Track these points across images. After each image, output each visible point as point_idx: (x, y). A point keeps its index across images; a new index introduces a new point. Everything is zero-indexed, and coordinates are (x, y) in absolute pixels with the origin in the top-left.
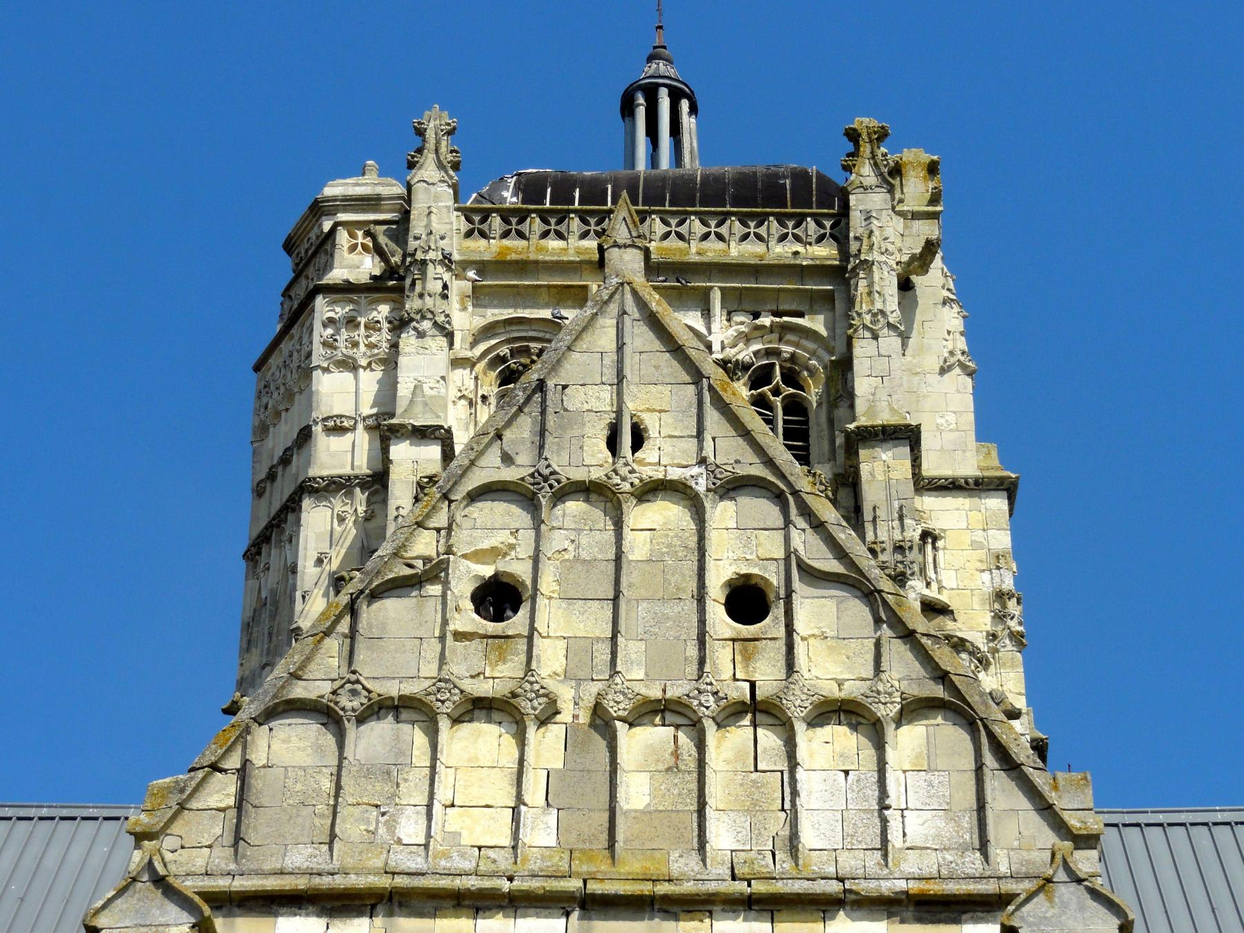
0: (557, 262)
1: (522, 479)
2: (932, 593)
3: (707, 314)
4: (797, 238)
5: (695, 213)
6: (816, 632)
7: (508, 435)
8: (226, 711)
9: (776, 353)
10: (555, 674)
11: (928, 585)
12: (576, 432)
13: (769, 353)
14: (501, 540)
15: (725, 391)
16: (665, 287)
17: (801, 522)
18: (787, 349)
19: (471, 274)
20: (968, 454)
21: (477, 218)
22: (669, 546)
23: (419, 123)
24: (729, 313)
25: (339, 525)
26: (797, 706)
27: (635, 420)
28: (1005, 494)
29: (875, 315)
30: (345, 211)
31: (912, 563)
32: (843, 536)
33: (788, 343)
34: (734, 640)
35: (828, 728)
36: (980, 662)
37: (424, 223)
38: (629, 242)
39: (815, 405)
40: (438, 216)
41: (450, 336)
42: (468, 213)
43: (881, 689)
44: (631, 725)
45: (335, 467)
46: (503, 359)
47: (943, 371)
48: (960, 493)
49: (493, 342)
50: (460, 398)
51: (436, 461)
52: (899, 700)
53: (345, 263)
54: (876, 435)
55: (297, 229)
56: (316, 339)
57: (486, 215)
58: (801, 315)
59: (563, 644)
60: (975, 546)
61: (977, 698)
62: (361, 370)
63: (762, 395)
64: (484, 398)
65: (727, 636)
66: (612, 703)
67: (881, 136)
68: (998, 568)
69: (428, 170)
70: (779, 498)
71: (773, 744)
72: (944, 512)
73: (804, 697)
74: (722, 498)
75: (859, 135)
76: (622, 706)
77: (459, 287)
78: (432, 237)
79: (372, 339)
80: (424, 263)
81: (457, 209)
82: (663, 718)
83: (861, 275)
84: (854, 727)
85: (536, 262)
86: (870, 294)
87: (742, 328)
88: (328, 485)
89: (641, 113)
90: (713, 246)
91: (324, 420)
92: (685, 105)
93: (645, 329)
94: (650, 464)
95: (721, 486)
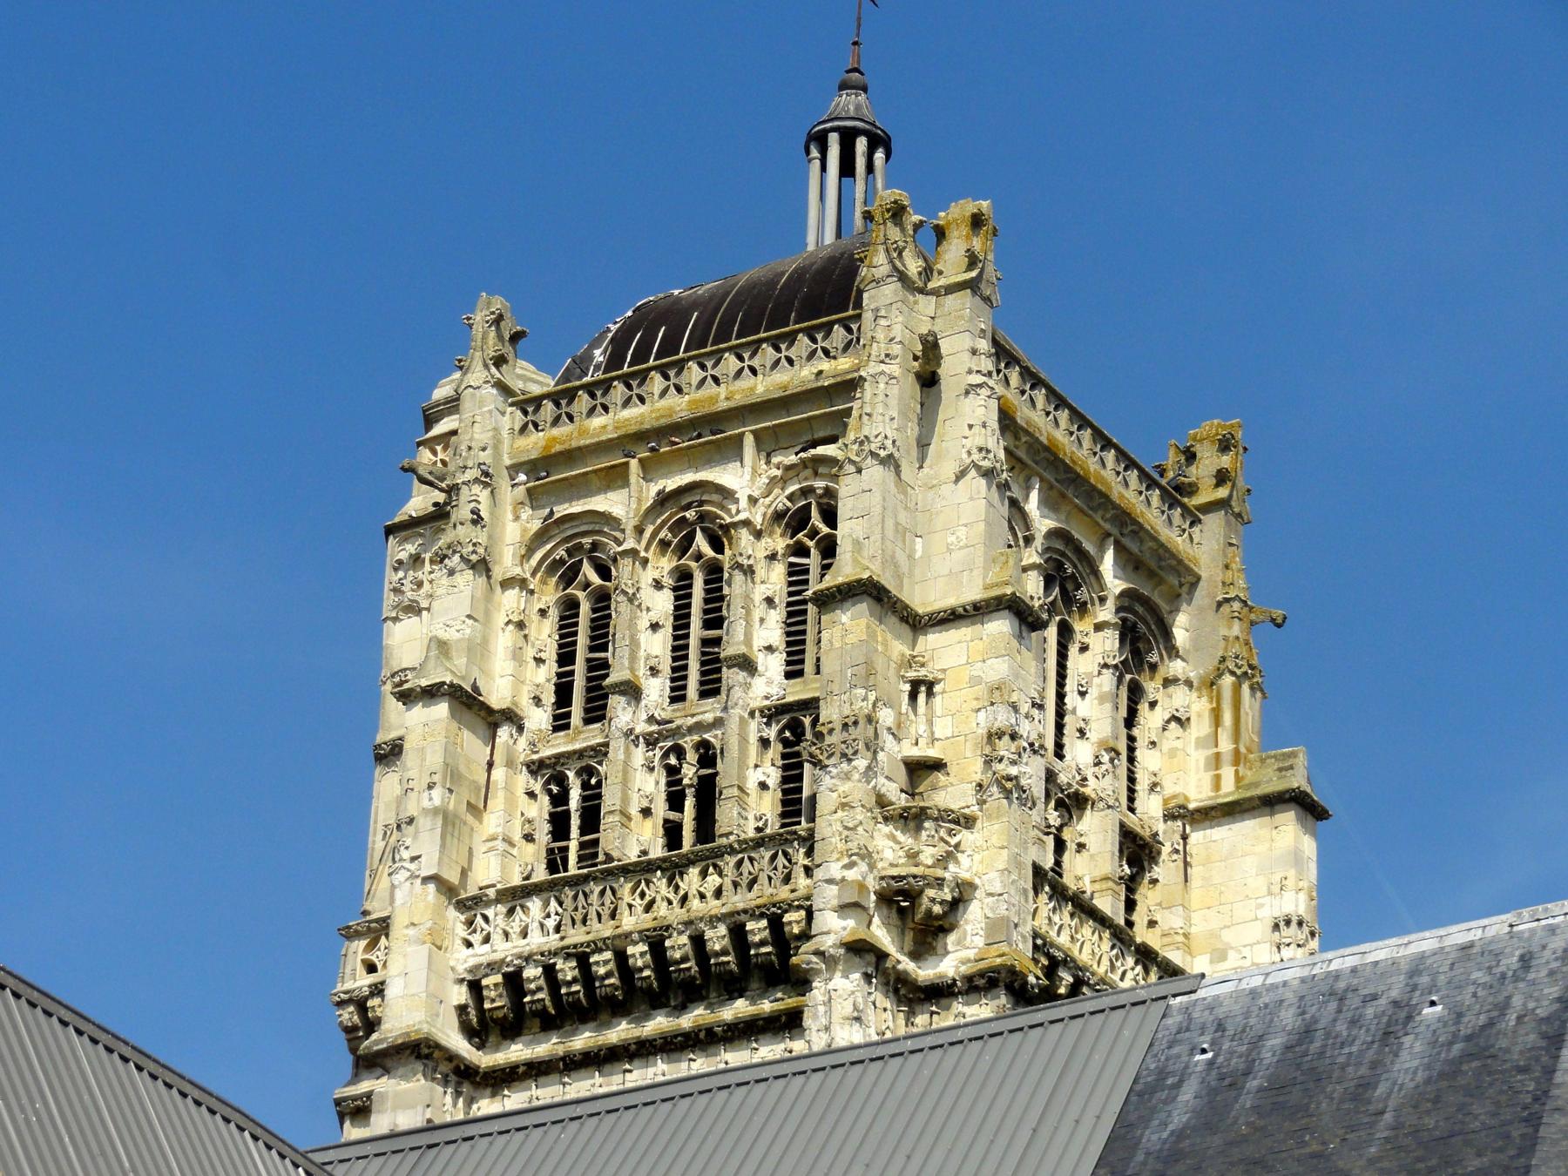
0: (599, 444)
5: (729, 349)
8: (937, 766)
13: (806, 492)
19: (522, 477)
20: (975, 572)
24: (768, 455)
36: (957, 823)
46: (562, 562)
48: (964, 622)
50: (507, 623)
54: (833, 596)
60: (975, 681)
63: (799, 543)
69: (477, 375)
72: (946, 651)
77: (510, 494)
81: (512, 405)
85: (580, 448)
92: (861, 144)
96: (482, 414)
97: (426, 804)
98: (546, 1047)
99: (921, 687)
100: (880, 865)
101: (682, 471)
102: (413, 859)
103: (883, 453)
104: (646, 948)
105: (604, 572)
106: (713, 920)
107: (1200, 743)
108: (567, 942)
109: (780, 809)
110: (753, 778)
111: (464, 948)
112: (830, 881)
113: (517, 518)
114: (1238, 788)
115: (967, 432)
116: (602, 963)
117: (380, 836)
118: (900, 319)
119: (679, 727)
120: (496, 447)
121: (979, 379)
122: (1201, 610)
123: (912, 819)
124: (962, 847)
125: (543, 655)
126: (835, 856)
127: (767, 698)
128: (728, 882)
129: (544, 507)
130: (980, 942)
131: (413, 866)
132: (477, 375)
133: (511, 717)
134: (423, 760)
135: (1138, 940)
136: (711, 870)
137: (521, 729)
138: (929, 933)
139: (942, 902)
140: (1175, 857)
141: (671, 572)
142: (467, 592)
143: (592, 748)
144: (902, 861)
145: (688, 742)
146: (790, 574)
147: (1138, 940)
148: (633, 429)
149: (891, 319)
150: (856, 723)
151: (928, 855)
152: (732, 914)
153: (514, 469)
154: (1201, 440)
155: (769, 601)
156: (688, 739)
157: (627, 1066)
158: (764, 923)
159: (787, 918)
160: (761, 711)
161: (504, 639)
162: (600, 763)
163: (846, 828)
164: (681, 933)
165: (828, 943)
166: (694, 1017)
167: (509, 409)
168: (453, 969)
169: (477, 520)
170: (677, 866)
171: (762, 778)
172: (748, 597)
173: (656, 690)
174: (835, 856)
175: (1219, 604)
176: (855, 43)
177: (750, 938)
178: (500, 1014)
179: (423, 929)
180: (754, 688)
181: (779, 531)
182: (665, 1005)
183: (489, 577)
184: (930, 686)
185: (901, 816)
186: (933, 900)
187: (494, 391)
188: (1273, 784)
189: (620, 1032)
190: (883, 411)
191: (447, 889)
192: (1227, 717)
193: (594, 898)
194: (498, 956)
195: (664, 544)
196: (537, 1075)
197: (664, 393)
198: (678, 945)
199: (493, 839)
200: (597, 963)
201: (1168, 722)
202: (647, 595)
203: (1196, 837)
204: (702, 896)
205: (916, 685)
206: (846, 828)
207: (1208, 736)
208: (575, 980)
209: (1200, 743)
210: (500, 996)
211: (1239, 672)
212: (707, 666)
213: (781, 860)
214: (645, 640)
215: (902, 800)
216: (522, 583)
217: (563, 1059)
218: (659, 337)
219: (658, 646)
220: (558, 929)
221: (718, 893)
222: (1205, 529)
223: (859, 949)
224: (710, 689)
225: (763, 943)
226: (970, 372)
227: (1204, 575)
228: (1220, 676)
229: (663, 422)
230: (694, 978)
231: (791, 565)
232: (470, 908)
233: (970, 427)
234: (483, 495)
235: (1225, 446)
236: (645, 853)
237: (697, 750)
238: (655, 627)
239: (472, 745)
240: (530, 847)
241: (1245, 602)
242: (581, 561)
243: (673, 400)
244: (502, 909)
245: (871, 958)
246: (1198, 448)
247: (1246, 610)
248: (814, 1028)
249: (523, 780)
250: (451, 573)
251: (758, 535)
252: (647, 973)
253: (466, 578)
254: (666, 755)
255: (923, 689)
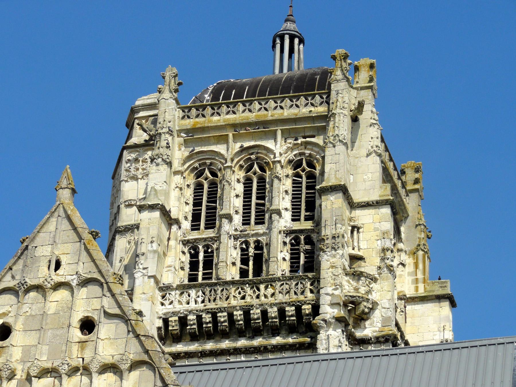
0: (216, 126)
1: (15, 286)
2: (356, 252)
3: (276, 141)
4: (312, 105)
6: (107, 337)
7: (14, 268)
8: (360, 258)
9: (304, 154)
10: (17, 360)
11: (353, 249)
12: (37, 265)
13: (301, 154)
14: (6, 309)
15: (89, 244)
16: (259, 131)
17: (108, 294)
18: (307, 152)
20: (376, 190)
21: (186, 111)
22: (62, 307)
23: (163, 74)
24: (285, 139)
25: (129, 245)
26: (94, 367)
27: (58, 258)
28: (389, 206)
29: (335, 137)
30: (143, 111)
31: (338, 243)
32: (121, 299)
33: (308, 149)
34: (79, 342)
35: (106, 374)
36: (372, 280)
37: (163, 116)
38: (66, 186)
39: (318, 174)
40: (170, 113)
41: (170, 164)
42: (183, 109)
43: (124, 358)
44: (39, 378)
45: (128, 221)
46: (196, 168)
47: (368, 156)
48: (370, 207)
49: (192, 162)
50: (176, 188)
51: (157, 218)
52: (130, 362)
53: (137, 135)
54: (328, 190)
55: (128, 119)
56: (123, 169)
57: (190, 109)
58: (313, 136)
59: (21, 348)
60: (376, 229)
61: (157, 359)
62: (139, 180)
63: (298, 173)
64: (188, 186)
65: (77, 341)
66: (32, 371)
67: (345, 57)
68: (384, 238)
69: (167, 94)
70: (101, 285)
71: (86, 382)
72: (363, 217)
73: (97, 364)
74: (82, 287)
75: (336, 58)
76: (36, 371)
77: (178, 140)
78: (165, 122)
79: (144, 167)
80: (160, 134)
81: (179, 108)
82: (51, 375)
83: (332, 120)
84: (115, 373)
85: (208, 127)
86: (334, 127)
87: (289, 145)
88: (125, 229)
89: (278, 46)
90: (279, 111)
91: (125, 202)
92: (296, 41)
93: (66, 221)
94: (61, 275)
95: (81, 282)
96: (169, 109)
97: (150, 248)
98: (194, 347)
99: (355, 229)
100: (344, 291)
101: (249, 141)
102: (144, 269)
103: (345, 141)
104: (242, 313)
105: (214, 174)
106: (272, 305)
107: (409, 274)
108: (207, 307)
109: (290, 269)
110: (280, 256)
111: (160, 306)
112: (327, 294)
113: (180, 150)
114: (425, 291)
115: (371, 140)
116: (222, 317)
117: (118, 261)
118: (347, 95)
119: (248, 234)
120: (174, 121)
121: (374, 122)
122: (409, 227)
123: (357, 275)
124: (373, 289)
125: (188, 202)
126: (330, 285)
127: (285, 227)
128: (277, 291)
129: (190, 147)
130: (379, 325)
131: (144, 271)
132: (167, 94)
133: (177, 222)
134: (149, 232)
135: (406, 339)
136: (269, 286)
137: (180, 228)
138: (361, 319)
139: (368, 308)
140: (402, 313)
141: (244, 177)
142: (165, 173)
143: (211, 238)
144: (352, 291)
145: (251, 240)
146: (293, 183)
147: (406, 339)
148: (231, 122)
149: (344, 96)
150: (338, 237)
151: (363, 290)
152: (280, 303)
153: (180, 131)
154: (407, 167)
155: (286, 192)
156: (251, 239)
157: (228, 358)
158: (294, 308)
159: (303, 307)
160: (284, 232)
161: (174, 194)
162: (213, 244)
163: (334, 275)
164: (257, 308)
165: (328, 317)
166: (258, 342)
167: (178, 110)
168: (157, 313)
169: (168, 147)
170: (255, 283)
171: (284, 256)
172: (279, 188)
173: (238, 219)
174: (330, 285)
175: (417, 226)
176: (291, 6)
177: (287, 313)
178: (175, 332)
179: (149, 295)
180: (280, 223)
181: (290, 167)
182: (245, 336)
183: (171, 169)
184: (358, 229)
185: (353, 274)
186: (364, 306)
187: (174, 101)
188: (440, 292)
189: (226, 344)
190: (341, 125)
191: (157, 282)
192: (421, 266)
193: (219, 292)
194: (177, 310)
195: (241, 167)
196: (188, 358)
197: (244, 111)
198: (256, 313)
199: (170, 266)
200: (220, 316)
201: (399, 265)
202: (235, 184)
203: (408, 307)
204: (266, 296)
205: (353, 227)
206: (334, 275)
207: (413, 272)
208: (210, 322)
209: (409, 274)
210: (176, 325)
211: (426, 250)
212: (258, 209)
213: (300, 286)
214: (233, 199)
215: (348, 269)
216: (182, 173)
217: (201, 352)
218: (227, 94)
219: (239, 203)
220: (203, 302)
221: (273, 295)
222: (410, 198)
223: (339, 320)
224: (260, 221)
225: (292, 316)
226: (371, 118)
227: (410, 214)
228: (418, 251)
229: (244, 121)
230: (260, 326)
231: (294, 180)
232: (164, 291)
233: (372, 138)
234: (170, 138)
235: (417, 170)
236: (233, 278)
237: (254, 243)
238: (237, 196)
239: (164, 228)
240: (182, 272)
241: (425, 226)
242: (205, 169)
243: (247, 114)
244: (178, 292)
245: (343, 324)
246: (406, 170)
247: (425, 229)
248: (321, 348)
249: (180, 247)
250: (157, 165)
251: (282, 167)
252: (241, 322)
253: (164, 168)
254: (241, 244)
255: (356, 229)
